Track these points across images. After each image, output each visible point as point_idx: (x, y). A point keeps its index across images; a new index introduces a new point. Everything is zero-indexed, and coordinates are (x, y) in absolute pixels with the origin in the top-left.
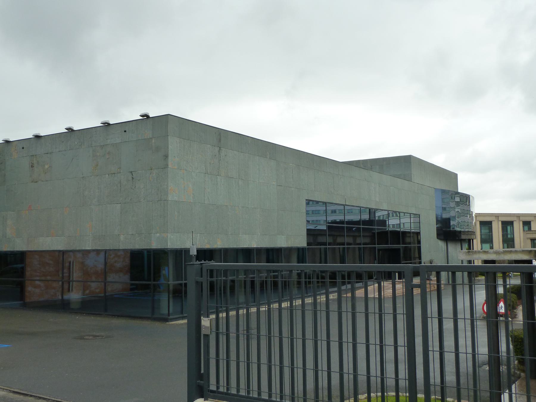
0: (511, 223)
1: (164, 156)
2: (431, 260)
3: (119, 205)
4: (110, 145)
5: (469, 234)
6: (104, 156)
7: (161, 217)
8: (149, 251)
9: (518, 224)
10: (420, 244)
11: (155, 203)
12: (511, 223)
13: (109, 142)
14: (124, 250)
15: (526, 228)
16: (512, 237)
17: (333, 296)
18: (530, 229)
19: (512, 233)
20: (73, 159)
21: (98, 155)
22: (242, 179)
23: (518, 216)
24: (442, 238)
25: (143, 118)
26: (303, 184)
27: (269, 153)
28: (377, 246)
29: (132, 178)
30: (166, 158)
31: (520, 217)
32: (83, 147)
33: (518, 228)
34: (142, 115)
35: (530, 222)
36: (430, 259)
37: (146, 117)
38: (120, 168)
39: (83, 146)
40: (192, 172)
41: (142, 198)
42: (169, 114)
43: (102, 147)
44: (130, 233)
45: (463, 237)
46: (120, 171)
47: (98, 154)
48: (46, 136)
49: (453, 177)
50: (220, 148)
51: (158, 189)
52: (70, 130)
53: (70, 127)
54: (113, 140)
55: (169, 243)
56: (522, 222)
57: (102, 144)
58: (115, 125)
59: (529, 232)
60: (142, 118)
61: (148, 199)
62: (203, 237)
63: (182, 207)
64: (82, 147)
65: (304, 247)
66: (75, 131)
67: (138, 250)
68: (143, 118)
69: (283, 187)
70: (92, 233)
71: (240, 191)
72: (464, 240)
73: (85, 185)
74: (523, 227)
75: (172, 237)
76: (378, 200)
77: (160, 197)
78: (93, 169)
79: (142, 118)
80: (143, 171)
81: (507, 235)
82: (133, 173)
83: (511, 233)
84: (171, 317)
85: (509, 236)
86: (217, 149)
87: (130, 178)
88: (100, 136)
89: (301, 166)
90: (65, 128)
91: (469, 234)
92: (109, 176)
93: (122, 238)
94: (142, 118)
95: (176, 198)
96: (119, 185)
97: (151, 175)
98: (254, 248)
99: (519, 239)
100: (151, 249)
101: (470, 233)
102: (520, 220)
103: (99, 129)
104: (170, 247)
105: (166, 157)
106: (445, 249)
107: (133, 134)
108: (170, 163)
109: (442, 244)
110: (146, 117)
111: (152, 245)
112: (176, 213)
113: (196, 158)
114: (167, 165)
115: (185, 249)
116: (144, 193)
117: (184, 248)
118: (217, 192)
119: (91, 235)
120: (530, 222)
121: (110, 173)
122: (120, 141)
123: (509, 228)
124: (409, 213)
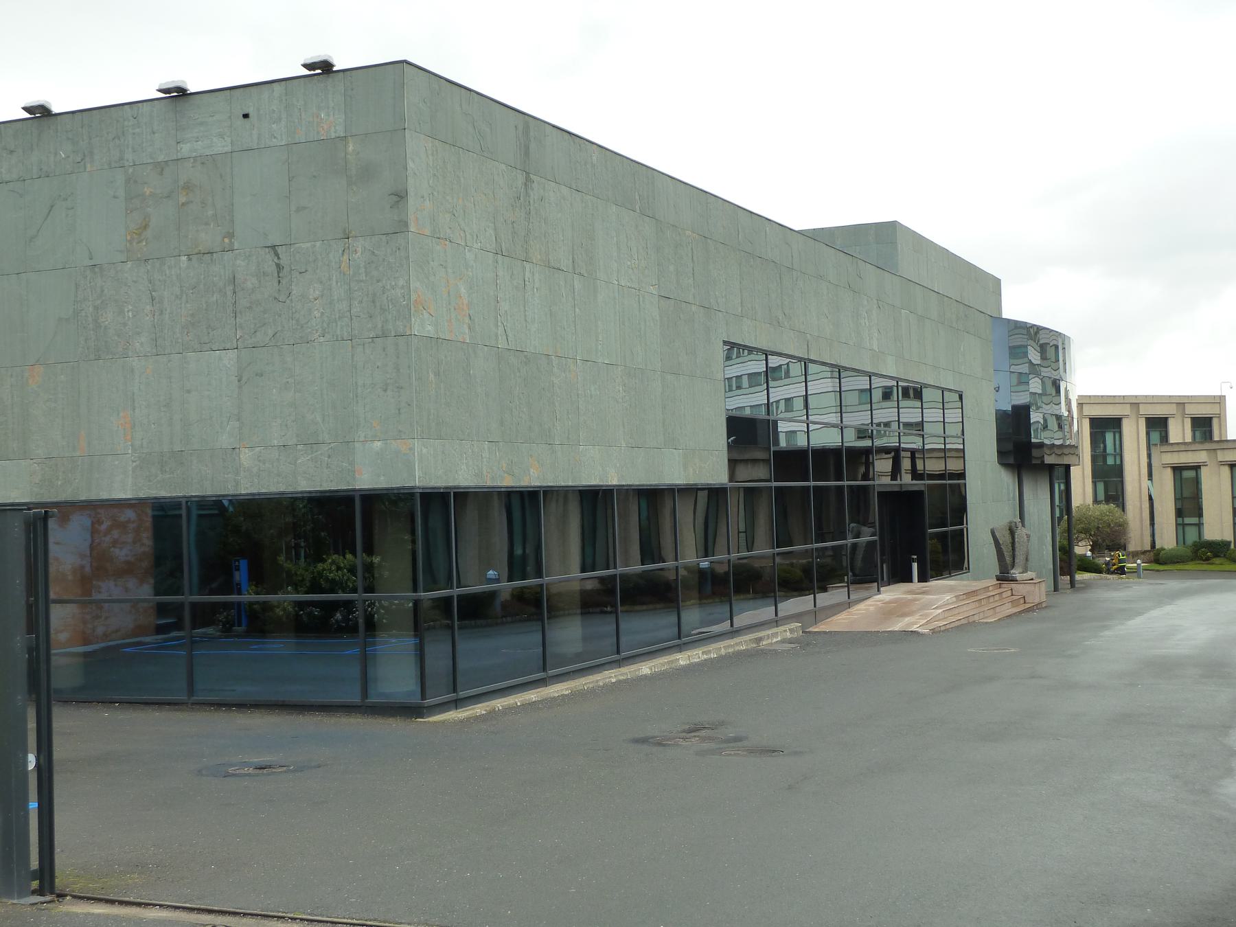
0: (1115, 424)
1: (389, 195)
2: (1011, 523)
3: (232, 354)
4: (192, 160)
5: (1070, 453)
6: (168, 197)
7: (385, 390)
8: (188, 499)
9: (1135, 427)
10: (965, 479)
11: (364, 345)
12: (1115, 424)
13: (185, 149)
14: (137, 504)
15: (1155, 436)
16: (1118, 462)
17: (791, 631)
18: (1165, 439)
19: (1118, 451)
20: (52, 206)
21: (148, 193)
22: (580, 274)
23: (1135, 403)
24: (1011, 461)
25: (312, 72)
26: (717, 293)
27: (640, 196)
28: (812, 483)
29: (278, 265)
30: (398, 202)
31: (1141, 406)
32: (88, 168)
33: (1133, 437)
34: (28, 105)
35: (1166, 419)
36: (1008, 521)
37: (319, 71)
38: (231, 235)
39: (88, 166)
40: (465, 249)
41: (317, 331)
42: (406, 62)
43: (160, 167)
44: (276, 442)
45: (1049, 460)
46: (231, 243)
47: (147, 191)
48: (276, 86)
49: (993, 285)
50: (528, 173)
51: (374, 302)
52: (40, 113)
53: (41, 103)
54: (200, 142)
55: (419, 471)
56: (1189, 420)
57: (161, 158)
58: (208, 94)
59: (1165, 448)
60: (307, 72)
61: (339, 333)
62: (497, 454)
63: (446, 357)
64: (85, 168)
65: (722, 484)
66: (59, 117)
67: (318, 495)
68: (312, 72)
69: (672, 302)
70: (132, 445)
71: (577, 310)
72: (1051, 467)
73: (102, 291)
74: (1148, 434)
75: (425, 450)
76: (875, 347)
77: (383, 327)
78: (129, 238)
79: (307, 72)
80: (318, 244)
81: (1104, 457)
82: (279, 250)
83: (1115, 451)
84: (428, 702)
85: (1110, 461)
86: (521, 178)
87: (270, 267)
88: (154, 133)
89: (711, 239)
90: (23, 106)
91: (1063, 454)
92: (190, 260)
93: (246, 457)
94: (163, 95)
95: (429, 330)
96: (229, 290)
97: (346, 257)
98: (614, 486)
99: (1136, 468)
100: (354, 490)
101: (1066, 451)
102: (1184, 415)
103: (146, 107)
104: (421, 484)
105: (400, 196)
106: (1014, 495)
107: (274, 126)
108: (411, 218)
109: (1006, 479)
110: (319, 71)
111: (357, 476)
112: (432, 376)
113: (474, 205)
114: (406, 224)
115: (456, 490)
116: (322, 313)
117: (455, 487)
118: (525, 310)
119: (130, 451)
120: (1166, 419)
121: (196, 251)
122: (229, 149)
123: (1109, 437)
124: (938, 388)
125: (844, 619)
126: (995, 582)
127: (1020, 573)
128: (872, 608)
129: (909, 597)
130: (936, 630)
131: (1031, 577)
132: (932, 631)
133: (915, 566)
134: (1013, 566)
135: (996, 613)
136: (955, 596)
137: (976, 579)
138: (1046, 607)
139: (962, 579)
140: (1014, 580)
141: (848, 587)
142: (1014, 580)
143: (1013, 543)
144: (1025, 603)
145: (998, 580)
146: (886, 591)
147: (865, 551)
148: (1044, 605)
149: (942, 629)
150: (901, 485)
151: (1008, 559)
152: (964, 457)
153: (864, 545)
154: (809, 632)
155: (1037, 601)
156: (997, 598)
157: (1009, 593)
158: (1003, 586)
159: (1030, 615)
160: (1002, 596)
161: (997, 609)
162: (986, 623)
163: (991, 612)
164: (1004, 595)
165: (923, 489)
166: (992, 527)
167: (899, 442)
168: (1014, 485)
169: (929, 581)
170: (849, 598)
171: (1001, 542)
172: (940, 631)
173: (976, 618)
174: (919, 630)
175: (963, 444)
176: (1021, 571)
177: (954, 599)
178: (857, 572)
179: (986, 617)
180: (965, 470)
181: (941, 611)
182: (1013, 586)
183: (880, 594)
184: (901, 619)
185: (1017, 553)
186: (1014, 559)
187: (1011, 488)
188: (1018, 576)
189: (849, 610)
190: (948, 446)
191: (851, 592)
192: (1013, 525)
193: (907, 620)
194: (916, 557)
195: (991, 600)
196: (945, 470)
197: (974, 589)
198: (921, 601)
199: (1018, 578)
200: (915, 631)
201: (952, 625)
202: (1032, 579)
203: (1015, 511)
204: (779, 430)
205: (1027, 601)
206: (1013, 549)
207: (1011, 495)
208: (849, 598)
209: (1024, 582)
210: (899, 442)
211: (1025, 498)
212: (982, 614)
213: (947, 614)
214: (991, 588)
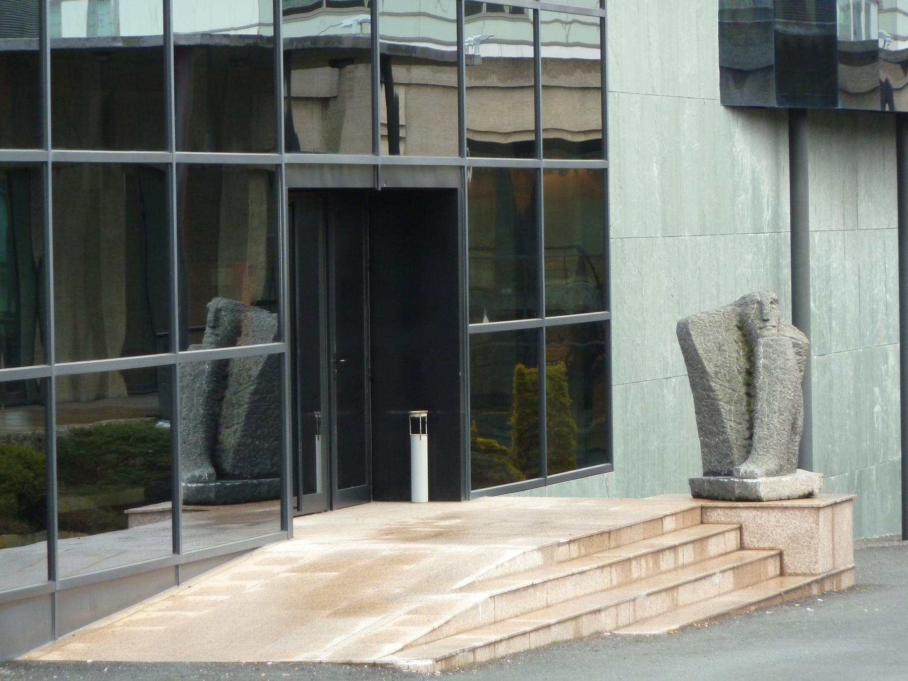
2: (744, 303)
28: (51, 154)
125: (151, 621)
126: (686, 501)
127: (769, 474)
128: (253, 587)
129: (388, 548)
130: (459, 661)
131: (805, 490)
132: (440, 666)
133: (420, 445)
134: (748, 450)
135: (676, 607)
136: (541, 549)
137: (630, 492)
138: (851, 589)
139: (584, 493)
140: (750, 498)
141: (174, 514)
142: (750, 498)
143: (750, 373)
144: (782, 573)
145: (697, 496)
146: (315, 529)
147: (255, 393)
148: (847, 581)
149: (483, 656)
150: (375, 167)
151: (732, 426)
152: (602, 89)
153: (256, 371)
154: (27, 666)
155: (822, 567)
156: (687, 555)
157: (732, 540)
158: (714, 515)
159: (792, 614)
160: (657, 564)
161: (684, 594)
162: (639, 639)
163: (660, 604)
164: (714, 547)
165: (451, 181)
166: (680, 318)
167: (536, 44)
168: (777, 178)
169: (467, 498)
170: (176, 549)
171: (710, 368)
172: (471, 666)
173: (606, 623)
174: (401, 661)
175: (603, 47)
176: (772, 465)
177: (537, 559)
178: (228, 463)
179: (644, 621)
180: (604, 130)
181: (485, 595)
182: (746, 515)
183: (290, 537)
184: (341, 622)
185: (762, 406)
186: (751, 427)
187: (766, 188)
188: (765, 485)
189: (175, 591)
190: (545, 52)
191: (183, 533)
192: (752, 311)
193: (365, 625)
194: (424, 414)
195: (667, 561)
196: (536, 131)
197: (607, 524)
198: (424, 563)
199: (763, 492)
200: (383, 666)
201: (519, 645)
202: (809, 495)
203: (777, 265)
204: (864, 38)
205: (790, 566)
206: (751, 394)
207: (767, 215)
208: (176, 549)
209: (782, 504)
210: (536, 44)
211: (812, 227)
212: (625, 614)
213: (506, 608)
214: (669, 524)
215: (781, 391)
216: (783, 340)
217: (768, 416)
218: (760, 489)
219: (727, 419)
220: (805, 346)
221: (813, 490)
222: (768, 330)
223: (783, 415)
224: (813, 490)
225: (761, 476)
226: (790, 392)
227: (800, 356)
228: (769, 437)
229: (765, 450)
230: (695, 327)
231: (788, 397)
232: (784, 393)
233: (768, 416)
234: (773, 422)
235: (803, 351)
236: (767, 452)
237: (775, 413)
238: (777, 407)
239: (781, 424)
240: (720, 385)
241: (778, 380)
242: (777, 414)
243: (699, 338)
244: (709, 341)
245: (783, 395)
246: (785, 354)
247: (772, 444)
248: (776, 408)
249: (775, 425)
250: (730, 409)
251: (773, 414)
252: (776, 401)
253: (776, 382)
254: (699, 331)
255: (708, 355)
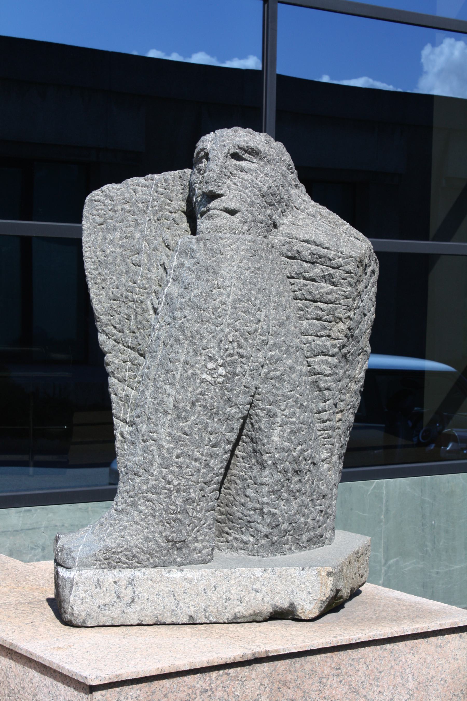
215: (186, 363)
216: (223, 242)
217: (149, 418)
218: (72, 598)
219: (125, 421)
220: (348, 264)
221: (292, 604)
222: (211, 217)
223: (186, 420)
224: (292, 604)
225: (84, 565)
226: (211, 365)
227: (334, 284)
228: (142, 471)
229: (129, 500)
230: (94, 212)
231: (204, 376)
232: (192, 366)
233: (149, 418)
234: (155, 435)
235: (337, 273)
236: (134, 504)
237: (166, 412)
238: (172, 400)
239: (176, 440)
240: (115, 340)
241: (184, 334)
242: (169, 417)
243: (93, 236)
244: (112, 242)
245: (190, 372)
246: (214, 273)
247: (144, 487)
248: (170, 402)
249: (160, 442)
250: (127, 396)
251: (159, 415)
252: (172, 384)
253: (177, 340)
254: (98, 219)
255: (99, 274)
